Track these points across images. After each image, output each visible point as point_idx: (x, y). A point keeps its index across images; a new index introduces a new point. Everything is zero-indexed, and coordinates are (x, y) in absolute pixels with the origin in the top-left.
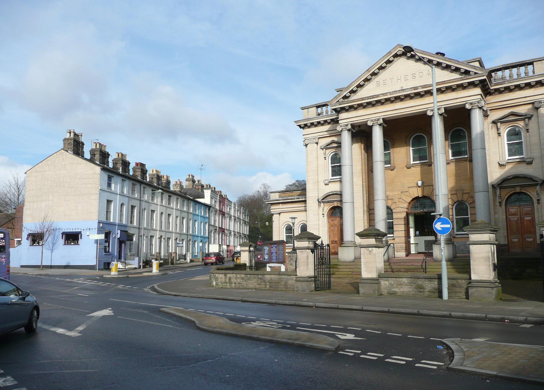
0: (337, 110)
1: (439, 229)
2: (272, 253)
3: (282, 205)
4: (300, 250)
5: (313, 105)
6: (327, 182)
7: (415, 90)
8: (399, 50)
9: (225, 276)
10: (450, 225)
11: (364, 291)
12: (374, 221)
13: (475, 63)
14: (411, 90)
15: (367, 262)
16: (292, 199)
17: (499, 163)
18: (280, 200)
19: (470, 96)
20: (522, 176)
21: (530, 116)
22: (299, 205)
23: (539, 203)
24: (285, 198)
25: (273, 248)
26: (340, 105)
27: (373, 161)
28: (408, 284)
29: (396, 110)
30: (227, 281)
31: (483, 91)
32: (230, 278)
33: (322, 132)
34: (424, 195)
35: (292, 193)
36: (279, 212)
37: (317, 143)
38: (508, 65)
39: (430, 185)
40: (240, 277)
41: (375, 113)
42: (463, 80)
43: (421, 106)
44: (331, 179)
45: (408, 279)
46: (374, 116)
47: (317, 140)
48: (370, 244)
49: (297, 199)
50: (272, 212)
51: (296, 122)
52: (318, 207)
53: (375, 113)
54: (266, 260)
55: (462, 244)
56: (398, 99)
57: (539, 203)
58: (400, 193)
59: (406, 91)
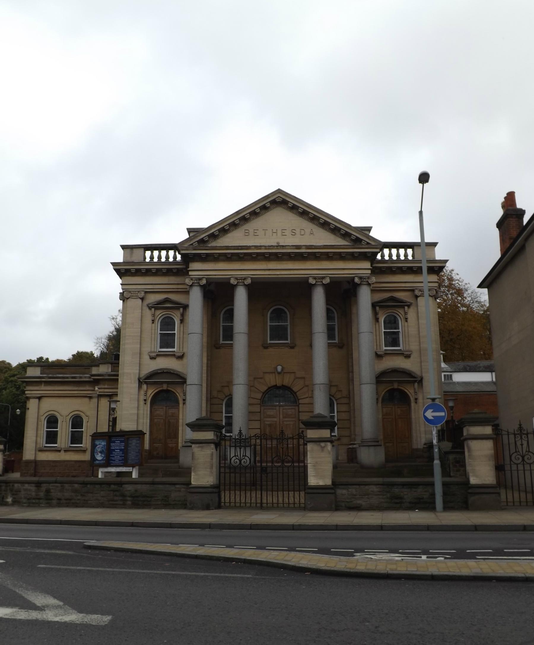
1: (430, 418)
2: (114, 450)
6: (153, 355)
8: (279, 197)
9: (36, 486)
15: (316, 463)
21: (409, 304)
23: (416, 402)
24: (50, 375)
27: (234, 332)
28: (379, 493)
30: (42, 494)
32: (48, 491)
34: (284, 384)
37: (142, 299)
40: (70, 488)
44: (159, 351)
45: (378, 486)
47: (142, 294)
50: (27, 395)
51: (113, 264)
52: (137, 391)
54: (97, 462)
57: (416, 402)
59: (286, 249)
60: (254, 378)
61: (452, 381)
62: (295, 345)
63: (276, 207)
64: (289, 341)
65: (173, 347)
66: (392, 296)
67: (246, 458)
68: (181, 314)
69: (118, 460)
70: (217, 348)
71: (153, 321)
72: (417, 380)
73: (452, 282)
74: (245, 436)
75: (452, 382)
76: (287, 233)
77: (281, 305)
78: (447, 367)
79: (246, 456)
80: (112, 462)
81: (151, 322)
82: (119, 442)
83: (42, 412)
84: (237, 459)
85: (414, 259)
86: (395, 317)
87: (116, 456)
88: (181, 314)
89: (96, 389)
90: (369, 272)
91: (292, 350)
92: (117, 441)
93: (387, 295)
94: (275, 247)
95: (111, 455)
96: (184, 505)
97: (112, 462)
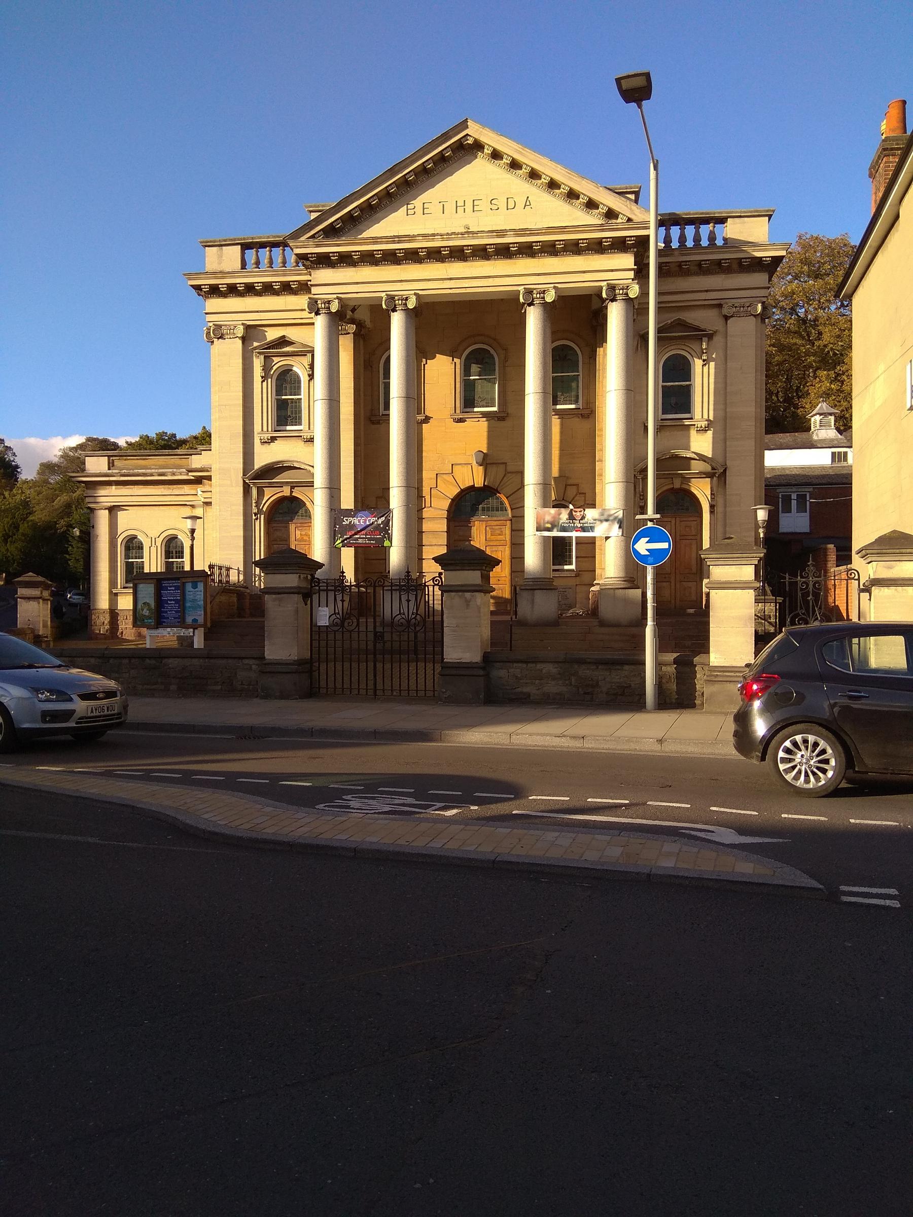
0: (330, 257)
1: (644, 552)
3: (116, 489)
5: (235, 240)
7: (498, 236)
10: (667, 543)
14: (488, 237)
19: (612, 271)
21: (711, 332)
22: (162, 490)
25: (167, 590)
26: (318, 246)
29: (451, 279)
33: (257, 312)
35: (144, 459)
36: (109, 504)
41: (401, 281)
42: (603, 230)
46: (398, 286)
53: (401, 281)
56: (458, 254)
59: (478, 238)
61: (847, 463)
63: (464, 156)
64: (495, 409)
68: (309, 365)
69: (173, 618)
70: (373, 423)
71: (264, 378)
72: (716, 473)
74: (349, 581)
75: (847, 465)
76: (484, 205)
78: (841, 439)
79: (417, 614)
84: (338, 618)
85: (727, 244)
87: (170, 611)
88: (309, 365)
89: (200, 493)
90: (631, 274)
91: (502, 424)
92: (171, 587)
96: (252, 692)
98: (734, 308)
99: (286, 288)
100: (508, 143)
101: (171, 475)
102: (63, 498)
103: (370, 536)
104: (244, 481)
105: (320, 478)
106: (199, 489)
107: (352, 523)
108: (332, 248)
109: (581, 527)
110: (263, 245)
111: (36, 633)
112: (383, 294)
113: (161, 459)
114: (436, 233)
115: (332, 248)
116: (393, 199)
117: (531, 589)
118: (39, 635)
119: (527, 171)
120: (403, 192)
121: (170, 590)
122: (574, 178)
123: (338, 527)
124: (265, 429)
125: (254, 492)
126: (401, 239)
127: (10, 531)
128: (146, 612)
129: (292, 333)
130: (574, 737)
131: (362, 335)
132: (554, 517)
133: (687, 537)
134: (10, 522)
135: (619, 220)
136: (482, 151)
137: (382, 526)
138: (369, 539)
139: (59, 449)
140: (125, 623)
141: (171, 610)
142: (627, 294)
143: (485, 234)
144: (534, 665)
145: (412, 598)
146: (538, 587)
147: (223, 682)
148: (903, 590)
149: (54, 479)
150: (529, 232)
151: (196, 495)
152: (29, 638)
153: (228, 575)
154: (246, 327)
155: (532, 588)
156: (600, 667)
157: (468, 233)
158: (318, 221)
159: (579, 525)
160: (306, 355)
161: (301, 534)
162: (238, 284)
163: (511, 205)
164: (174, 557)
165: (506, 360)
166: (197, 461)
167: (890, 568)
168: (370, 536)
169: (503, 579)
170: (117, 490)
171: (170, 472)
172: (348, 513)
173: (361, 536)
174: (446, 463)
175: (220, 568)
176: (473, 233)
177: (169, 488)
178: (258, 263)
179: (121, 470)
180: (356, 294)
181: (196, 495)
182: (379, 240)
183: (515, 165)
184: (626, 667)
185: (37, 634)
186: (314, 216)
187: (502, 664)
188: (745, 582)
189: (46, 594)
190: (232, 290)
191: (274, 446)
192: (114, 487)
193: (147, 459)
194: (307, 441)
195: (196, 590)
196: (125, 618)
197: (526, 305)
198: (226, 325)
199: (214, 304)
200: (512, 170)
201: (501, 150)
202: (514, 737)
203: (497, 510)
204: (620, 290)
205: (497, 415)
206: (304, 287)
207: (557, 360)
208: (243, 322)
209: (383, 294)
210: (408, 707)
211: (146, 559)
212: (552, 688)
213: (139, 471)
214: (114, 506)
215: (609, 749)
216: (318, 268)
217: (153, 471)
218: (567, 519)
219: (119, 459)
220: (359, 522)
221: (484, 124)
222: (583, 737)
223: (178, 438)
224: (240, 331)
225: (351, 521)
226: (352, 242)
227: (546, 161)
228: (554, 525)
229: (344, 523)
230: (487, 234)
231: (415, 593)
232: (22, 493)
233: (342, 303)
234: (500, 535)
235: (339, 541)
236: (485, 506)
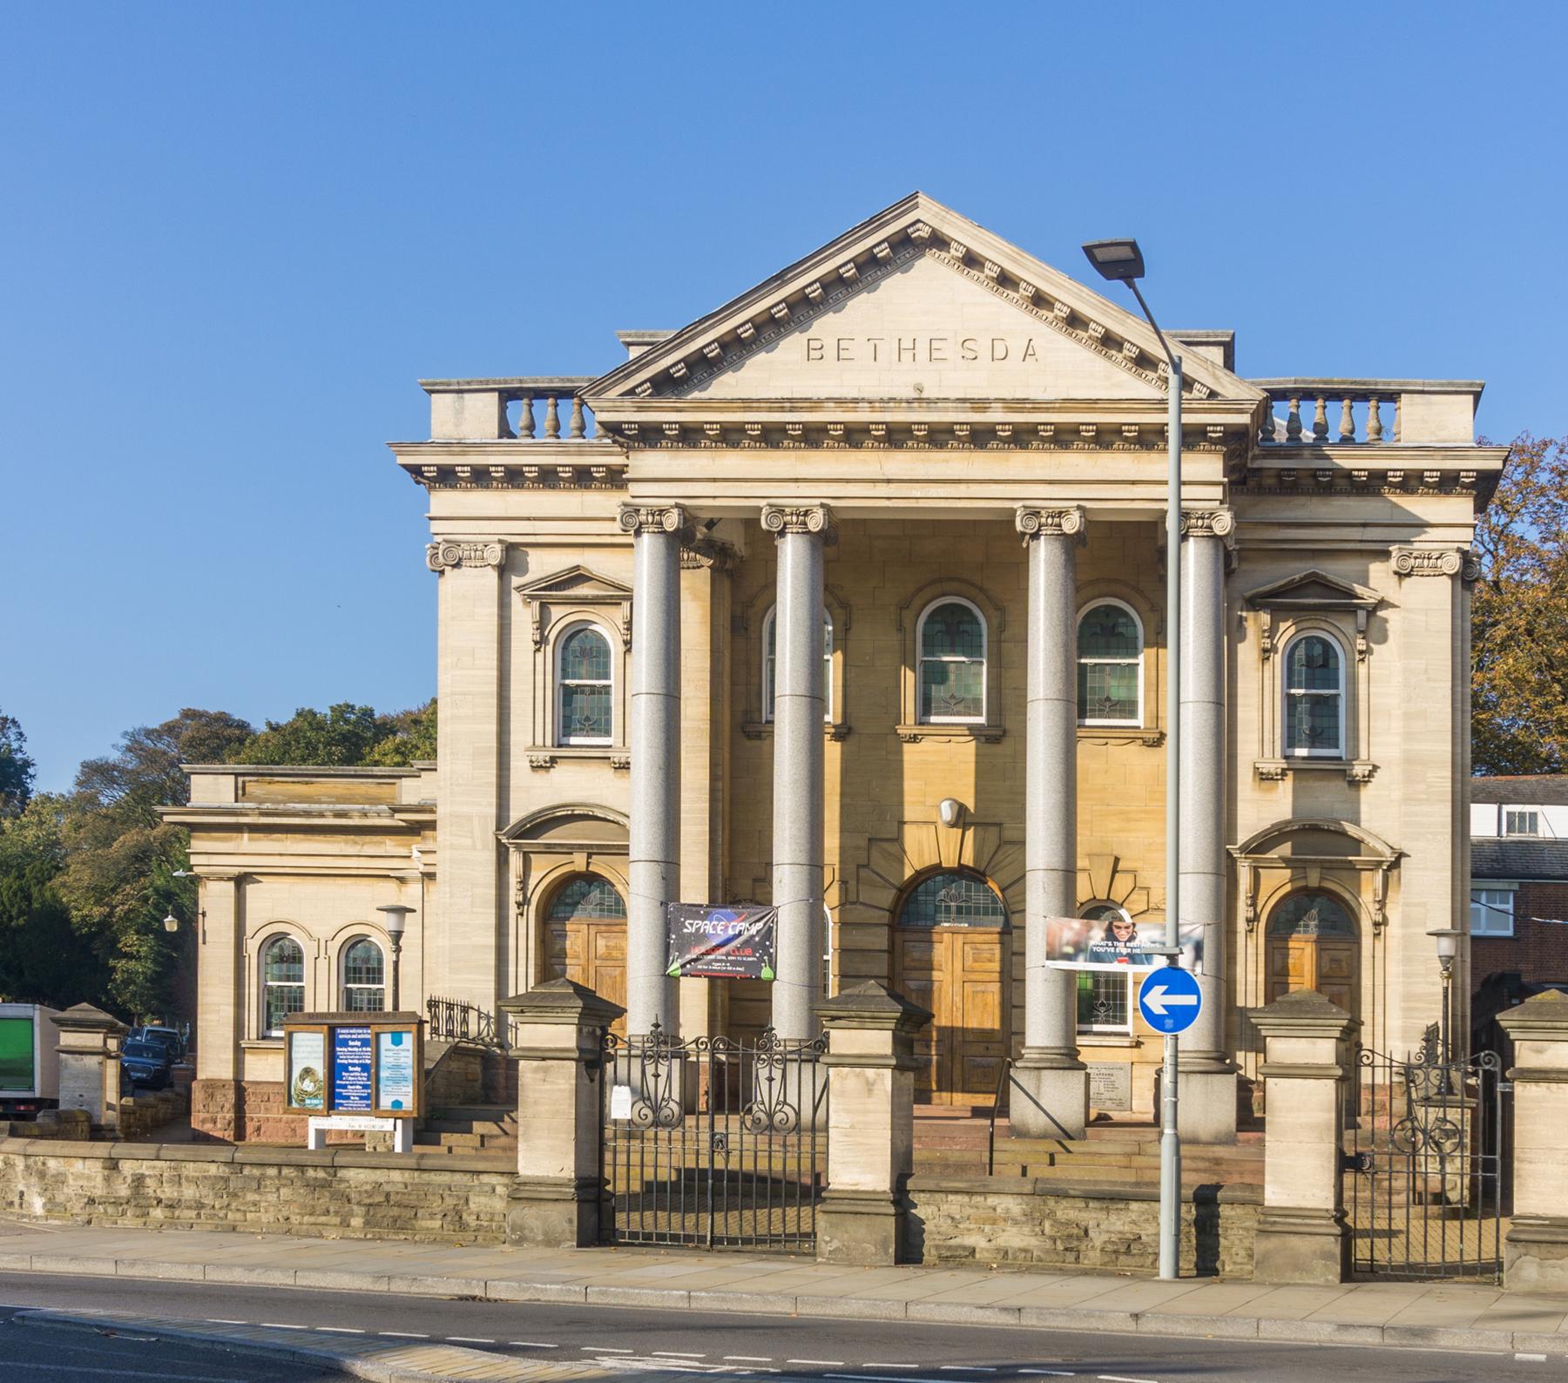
3: (250, 839)
4: (535, 1063)
7: (974, 410)
10: (1195, 997)
11: (835, 1244)
12: (1020, 958)
13: (1211, 348)
14: (956, 410)
16: (308, 814)
17: (1257, 765)
18: (247, 815)
20: (1332, 828)
25: (347, 1046)
26: (640, 409)
29: (889, 481)
30: (124, 1191)
31: (1228, 471)
32: (139, 1180)
33: (529, 519)
35: (307, 783)
36: (236, 871)
38: (1315, 386)
39: (989, 821)
41: (796, 480)
43: (994, 486)
46: (791, 490)
48: (1311, 1061)
49: (338, 815)
53: (796, 480)
55: (1096, 1071)
58: (864, 843)
59: (938, 410)
60: (869, 840)
62: (1005, 731)
64: (982, 720)
65: (607, 732)
66: (1314, 574)
67: (786, 1109)
68: (625, 623)
70: (749, 736)
71: (540, 643)
73: (107, 933)
76: (950, 350)
77: (944, 595)
79: (785, 1103)
80: (341, 1101)
81: (532, 647)
82: (359, 1043)
83: (250, 926)
86: (1326, 646)
88: (625, 623)
89: (416, 854)
90: (1218, 492)
92: (353, 1040)
93: (1298, 570)
94: (904, 405)
95: (338, 1082)
97: (341, 1101)
98: (1412, 560)
99: (582, 477)
100: (992, 242)
101: (360, 817)
102: (128, 840)
103: (734, 958)
104: (498, 840)
105: (643, 839)
106: (415, 846)
107: (702, 931)
108: (666, 415)
109: (1128, 955)
110: (540, 394)
111: (95, 1121)
112: (762, 503)
113: (340, 783)
114: (862, 396)
115: (666, 415)
116: (782, 330)
117: (1036, 1068)
118: (101, 1126)
119: (1027, 294)
120: (801, 318)
121: (352, 1047)
122: (1113, 313)
123: (674, 937)
124: (539, 741)
125: (515, 860)
126: (795, 405)
127: (13, 906)
128: (308, 1086)
129: (593, 561)
130: (1005, 1309)
131: (727, 570)
132: (1079, 934)
133: (1333, 980)
134: (14, 887)
135: (1195, 394)
136: (946, 249)
137: (757, 939)
138: (733, 963)
139: (122, 731)
140: (266, 1109)
141: (354, 1083)
142: (1210, 527)
143: (950, 405)
144: (983, 1199)
145: (777, 1074)
146: (1048, 1065)
147: (445, 1215)
148: (1559, 1088)
149: (110, 797)
150: (1030, 406)
151: (409, 857)
152: (82, 1131)
153: (465, 1021)
154: (507, 548)
155: (1038, 1065)
156: (1091, 1205)
157: (920, 400)
158: (641, 363)
159: (1124, 951)
160: (620, 604)
161: (607, 946)
162: (492, 466)
163: (1000, 353)
164: (364, 979)
165: (1002, 628)
166: (411, 791)
167: (1539, 1051)
168: (734, 958)
169: (995, 1046)
170: (253, 843)
171: (359, 811)
172: (694, 911)
173: (719, 958)
174: (888, 818)
175: (450, 1006)
176: (928, 401)
177: (356, 843)
178: (531, 427)
179: (260, 803)
180: (711, 500)
181: (409, 857)
182: (755, 405)
183: (1005, 280)
184: (1134, 1206)
185: (96, 1122)
186: (634, 352)
187: (928, 1195)
188: (1320, 1067)
189: (113, 1044)
190: (481, 477)
191: (560, 771)
192: (246, 836)
193: (312, 783)
194: (619, 768)
195: (400, 1047)
196: (266, 1098)
197: (1027, 537)
198: (468, 542)
199: (443, 501)
200: (1001, 289)
201: (979, 252)
202: (911, 1308)
203: (986, 914)
204: (1198, 518)
205: (984, 733)
206: (616, 478)
207: (1097, 634)
208: (501, 537)
209: (762, 503)
210: (760, 1265)
211: (307, 983)
212: (1015, 1238)
213: (296, 805)
214: (246, 874)
215: (1049, 1327)
216: (639, 449)
217: (324, 806)
218: (1103, 940)
219: (257, 781)
220: (714, 927)
221: (949, 202)
222: (1019, 1310)
223: (377, 715)
224: (495, 554)
225: (700, 928)
226: (704, 405)
227: (1060, 278)
228: (1079, 949)
229: (685, 930)
230: (954, 405)
231: (782, 1066)
232: (41, 823)
233: (687, 515)
234: (990, 961)
235: (676, 965)
236: (964, 904)
